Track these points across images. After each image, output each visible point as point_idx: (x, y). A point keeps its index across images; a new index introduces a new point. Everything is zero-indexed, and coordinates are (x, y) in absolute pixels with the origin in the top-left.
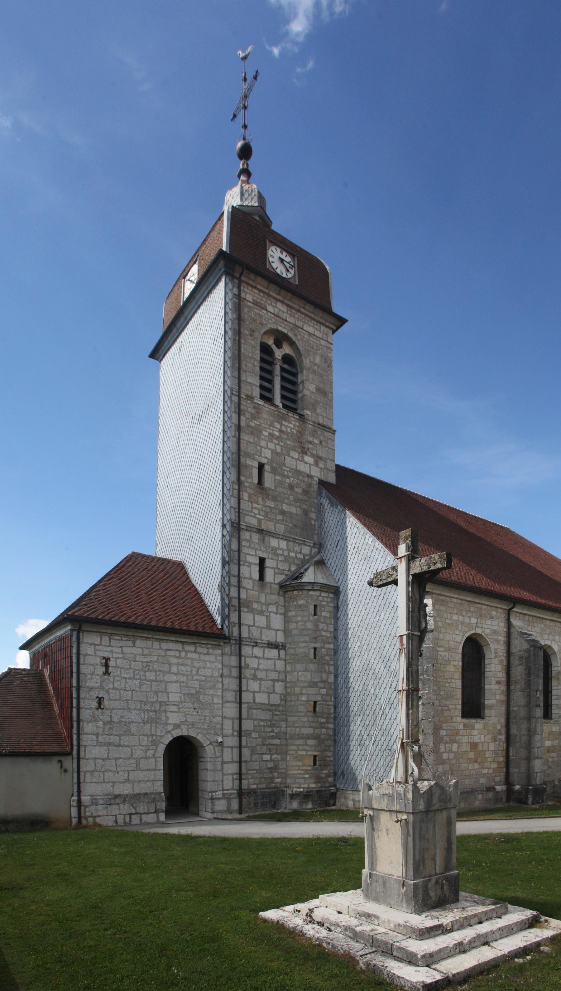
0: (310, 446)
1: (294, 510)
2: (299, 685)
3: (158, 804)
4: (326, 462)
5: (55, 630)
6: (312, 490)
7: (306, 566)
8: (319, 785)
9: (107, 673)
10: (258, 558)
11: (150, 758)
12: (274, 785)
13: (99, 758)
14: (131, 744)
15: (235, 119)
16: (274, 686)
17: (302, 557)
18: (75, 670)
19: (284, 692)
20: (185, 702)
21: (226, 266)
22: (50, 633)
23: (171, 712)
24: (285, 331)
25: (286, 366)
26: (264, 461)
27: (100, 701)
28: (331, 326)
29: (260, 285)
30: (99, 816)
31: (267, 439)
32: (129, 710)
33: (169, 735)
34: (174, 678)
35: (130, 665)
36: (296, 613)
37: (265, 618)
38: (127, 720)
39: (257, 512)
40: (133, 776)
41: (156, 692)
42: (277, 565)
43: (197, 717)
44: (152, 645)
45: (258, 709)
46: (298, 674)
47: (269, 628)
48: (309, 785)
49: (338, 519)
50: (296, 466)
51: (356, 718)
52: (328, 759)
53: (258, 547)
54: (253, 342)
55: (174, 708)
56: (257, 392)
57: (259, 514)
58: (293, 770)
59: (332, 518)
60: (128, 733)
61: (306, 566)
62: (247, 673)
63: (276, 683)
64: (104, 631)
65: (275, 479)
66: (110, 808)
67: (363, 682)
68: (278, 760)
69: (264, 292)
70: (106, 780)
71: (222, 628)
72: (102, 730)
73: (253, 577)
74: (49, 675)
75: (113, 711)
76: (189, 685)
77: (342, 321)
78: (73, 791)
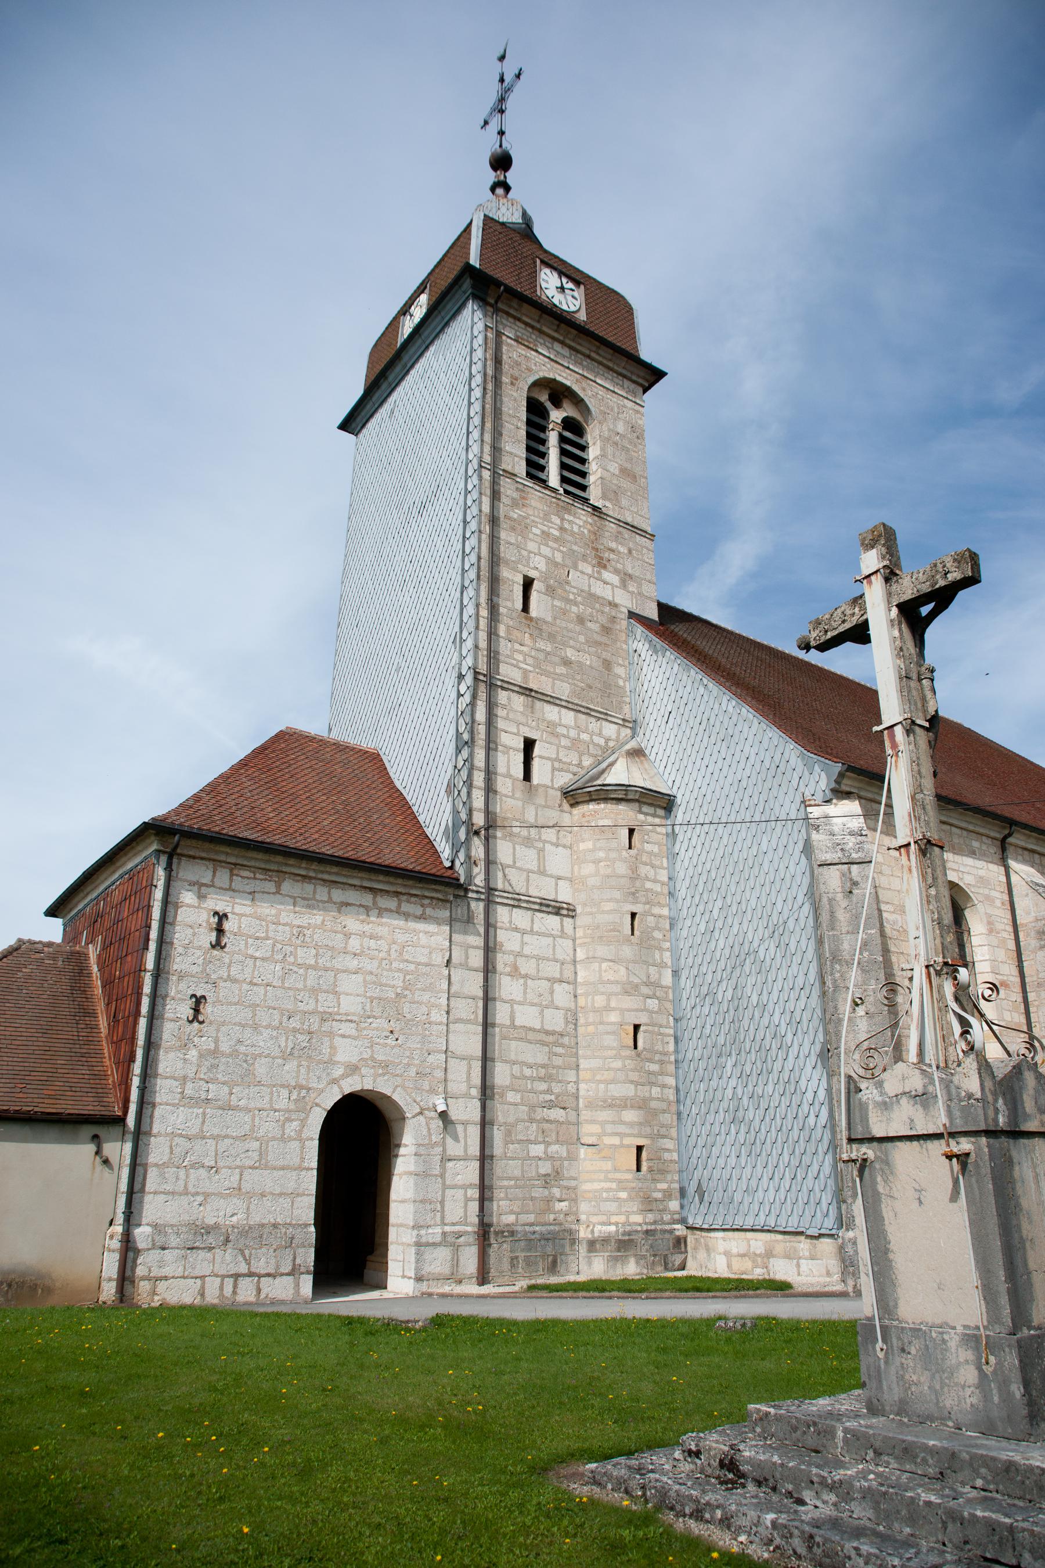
0: (612, 556)
1: (587, 660)
2: (602, 990)
3: (301, 1251)
4: (640, 585)
5: (123, 859)
6: (618, 627)
7: (611, 759)
8: (650, 1217)
9: (218, 945)
10: (522, 740)
11: (290, 1139)
12: (552, 1217)
13: (181, 1136)
14: (252, 1105)
15: (487, 127)
16: (552, 992)
17: (602, 742)
18: (154, 934)
19: (572, 1006)
20: (374, 1017)
21: (473, 287)
22: (112, 869)
23: (343, 1036)
24: (568, 383)
25: (567, 434)
26: (532, 574)
27: (198, 1002)
28: (640, 381)
29: (527, 316)
30: (166, 1278)
31: (539, 539)
32: (256, 1027)
33: (335, 1088)
34: (354, 964)
35: (267, 931)
36: (594, 845)
37: (535, 851)
38: (251, 1050)
39: (520, 658)
40: (253, 1180)
41: (315, 991)
42: (558, 753)
43: (396, 1050)
44: (315, 892)
45: (521, 1039)
46: (600, 967)
47: (542, 872)
48: (628, 1218)
49: (667, 675)
50: (590, 586)
51: (723, 1059)
52: (666, 1156)
53: (523, 720)
54: (515, 394)
55: (347, 1028)
56: (521, 468)
57: (525, 662)
58: (592, 1181)
59: (656, 673)
60: (248, 1079)
61: (611, 759)
62: (502, 961)
63: (556, 986)
64: (222, 858)
65: (553, 606)
66: (192, 1256)
67: (733, 982)
68: (561, 1159)
69: (533, 327)
70: (191, 1189)
71: (451, 868)
72: (194, 1070)
73: (512, 772)
74: (99, 956)
75: (223, 1029)
76: (384, 981)
77: (655, 375)
78: (115, 1212)
